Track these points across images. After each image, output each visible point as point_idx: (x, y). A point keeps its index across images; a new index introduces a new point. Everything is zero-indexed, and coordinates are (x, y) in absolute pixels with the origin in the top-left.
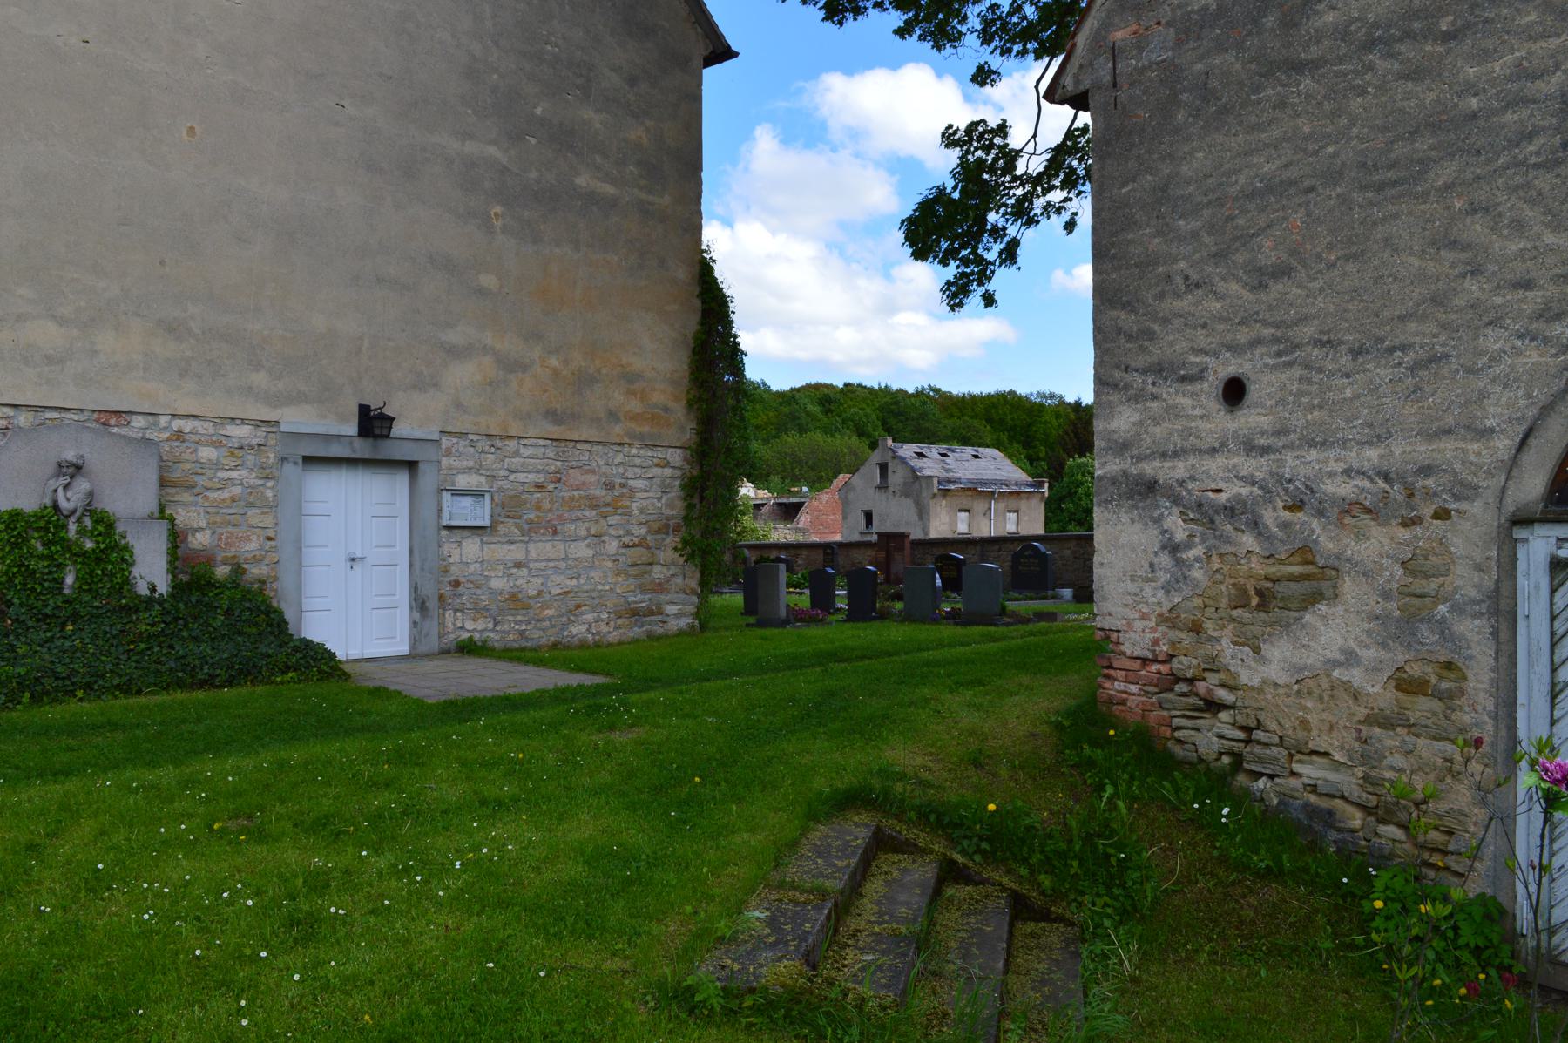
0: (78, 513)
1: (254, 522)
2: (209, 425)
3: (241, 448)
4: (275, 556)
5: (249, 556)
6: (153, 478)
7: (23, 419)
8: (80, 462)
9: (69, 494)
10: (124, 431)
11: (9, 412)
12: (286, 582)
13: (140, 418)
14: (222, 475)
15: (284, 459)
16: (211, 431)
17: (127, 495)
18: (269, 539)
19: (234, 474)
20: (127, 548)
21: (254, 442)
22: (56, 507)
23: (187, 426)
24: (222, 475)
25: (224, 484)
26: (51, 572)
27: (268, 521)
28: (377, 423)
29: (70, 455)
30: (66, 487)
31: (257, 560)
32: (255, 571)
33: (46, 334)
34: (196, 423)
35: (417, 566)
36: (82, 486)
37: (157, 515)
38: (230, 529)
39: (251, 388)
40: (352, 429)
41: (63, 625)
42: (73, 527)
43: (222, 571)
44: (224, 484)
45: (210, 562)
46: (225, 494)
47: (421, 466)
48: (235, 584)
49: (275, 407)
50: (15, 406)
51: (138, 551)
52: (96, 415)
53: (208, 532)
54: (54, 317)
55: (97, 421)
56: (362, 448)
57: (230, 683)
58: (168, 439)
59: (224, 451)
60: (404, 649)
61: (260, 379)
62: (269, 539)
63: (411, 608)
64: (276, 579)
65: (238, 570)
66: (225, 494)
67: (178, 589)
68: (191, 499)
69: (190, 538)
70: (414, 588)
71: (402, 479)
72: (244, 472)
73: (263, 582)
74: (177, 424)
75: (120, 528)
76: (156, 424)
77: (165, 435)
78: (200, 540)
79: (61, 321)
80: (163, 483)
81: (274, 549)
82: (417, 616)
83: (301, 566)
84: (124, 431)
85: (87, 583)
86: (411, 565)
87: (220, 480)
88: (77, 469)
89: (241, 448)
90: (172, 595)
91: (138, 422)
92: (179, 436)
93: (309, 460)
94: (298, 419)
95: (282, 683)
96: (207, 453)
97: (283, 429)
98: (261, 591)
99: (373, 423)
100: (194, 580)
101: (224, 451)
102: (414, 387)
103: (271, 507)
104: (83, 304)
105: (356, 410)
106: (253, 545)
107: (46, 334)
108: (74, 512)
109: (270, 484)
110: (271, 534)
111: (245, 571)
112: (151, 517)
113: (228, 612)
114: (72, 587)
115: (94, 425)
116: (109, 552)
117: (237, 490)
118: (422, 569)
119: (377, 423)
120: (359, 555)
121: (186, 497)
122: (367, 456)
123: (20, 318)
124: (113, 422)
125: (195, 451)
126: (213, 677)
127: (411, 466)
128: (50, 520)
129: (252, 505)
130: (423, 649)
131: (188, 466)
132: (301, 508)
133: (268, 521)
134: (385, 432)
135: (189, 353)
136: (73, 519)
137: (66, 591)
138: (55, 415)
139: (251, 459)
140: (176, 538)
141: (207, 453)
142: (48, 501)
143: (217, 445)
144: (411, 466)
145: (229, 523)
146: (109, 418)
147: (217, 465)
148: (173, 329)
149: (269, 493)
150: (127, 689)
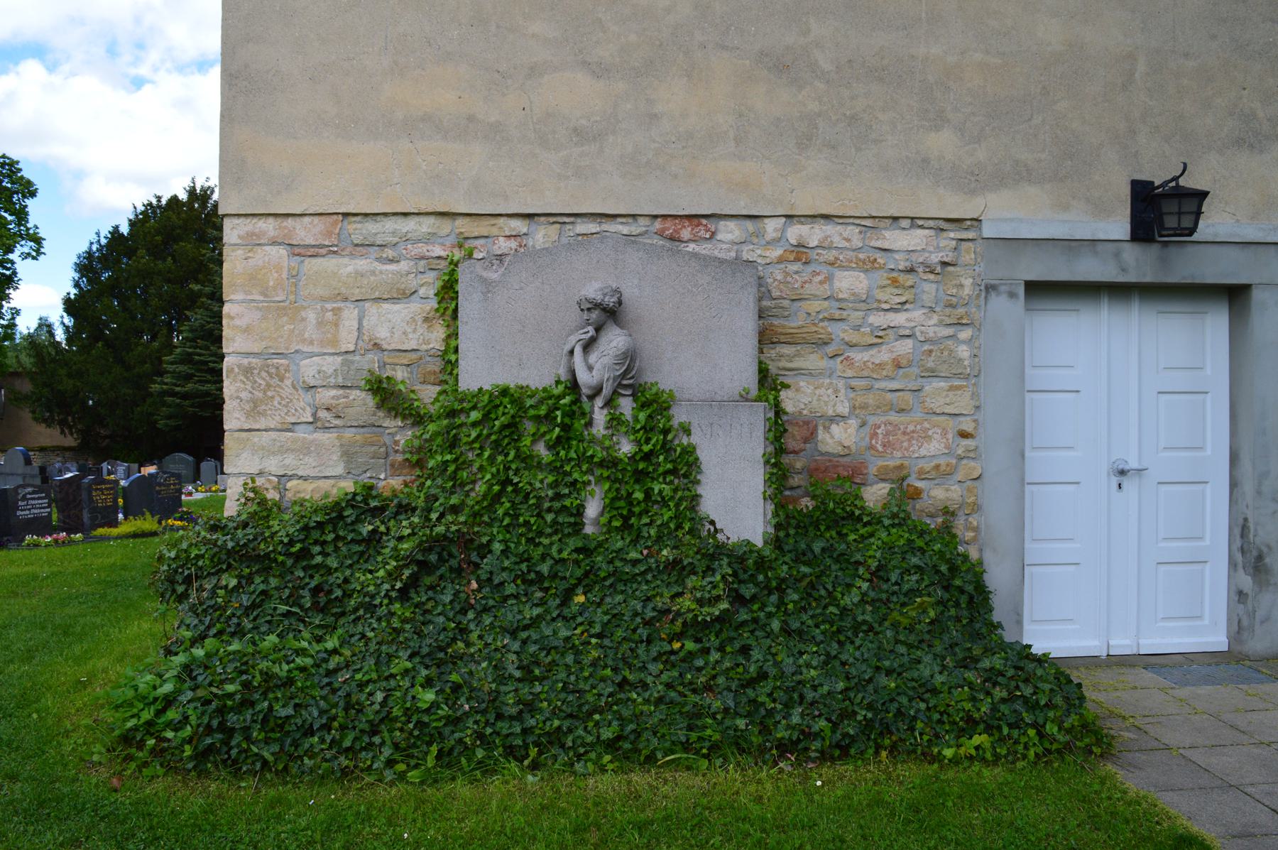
0: (607, 391)
1: (937, 403)
2: (851, 231)
3: (911, 270)
4: (975, 468)
5: (928, 466)
6: (748, 326)
7: (542, 236)
8: (610, 301)
9: (593, 358)
10: (704, 249)
11: (519, 226)
12: (996, 513)
13: (731, 224)
14: (877, 319)
15: (990, 288)
16: (857, 243)
17: (702, 361)
18: (964, 435)
19: (899, 319)
20: (689, 451)
21: (935, 258)
22: (574, 386)
23: (813, 234)
24: (877, 319)
25: (880, 337)
26: (558, 496)
27: (962, 403)
28: (1169, 206)
29: (592, 290)
30: (588, 346)
31: (941, 474)
32: (938, 494)
33: (573, 94)
34: (830, 229)
35: (1248, 487)
36: (614, 341)
37: (754, 392)
38: (893, 417)
39: (926, 161)
40: (1119, 227)
41: (568, 595)
42: (600, 416)
43: (875, 495)
44: (880, 337)
45: (854, 475)
46: (883, 355)
47: (1257, 295)
48: (900, 520)
49: (973, 192)
50: (530, 216)
51: (705, 455)
52: (658, 225)
53: (853, 423)
54: (585, 64)
55: (660, 234)
56: (1139, 264)
57: (841, 751)
58: (780, 260)
59: (881, 277)
60: (1217, 640)
61: (942, 143)
62: (964, 435)
63: (1233, 564)
64: (976, 508)
65: (905, 493)
66: (883, 355)
67: (788, 523)
68: (824, 363)
69: (821, 434)
70: (1241, 530)
71: (1214, 324)
72: (917, 314)
73: (948, 513)
74: (795, 232)
75: (679, 415)
76: (759, 234)
77: (777, 252)
78: (839, 438)
79: (599, 71)
80: (766, 338)
81: (972, 454)
82: (1246, 582)
83: (1022, 482)
84: (704, 249)
85: (623, 515)
86: (1234, 484)
87: (874, 329)
88: (609, 313)
89: (911, 270)
90: (777, 543)
91: (729, 232)
92: (800, 252)
93: (1038, 290)
94: (1013, 213)
95: (955, 761)
96: (849, 282)
97: (988, 231)
98: (947, 529)
99: (1161, 211)
100: (819, 512)
101: (881, 277)
102: (1239, 142)
103: (967, 376)
104: (633, 37)
105: (1126, 191)
106: (934, 447)
107: (573, 94)
108: (598, 391)
109: (965, 334)
110: (968, 426)
111: (916, 494)
112: (744, 398)
113: (879, 574)
114: (596, 522)
115: (657, 241)
116: (662, 462)
117: (906, 347)
118: (1259, 492)
119: (1169, 206)
120: (1133, 464)
121: (813, 361)
122: (1148, 279)
123: (534, 71)
124: (686, 234)
125: (829, 279)
126: (809, 735)
127: (1235, 296)
128: (565, 407)
129: (933, 374)
130: (1258, 644)
131: (815, 306)
132: (1022, 377)
133: (962, 403)
134: (1187, 222)
135: (813, 106)
136: (599, 402)
137: (589, 530)
138: (592, 227)
139: (929, 290)
140: (783, 438)
141: (849, 282)
142: (563, 373)
143: (869, 266)
144: (1235, 296)
145: (891, 407)
146: (681, 227)
147: (867, 303)
148: (783, 66)
149: (964, 352)
150: (627, 750)
